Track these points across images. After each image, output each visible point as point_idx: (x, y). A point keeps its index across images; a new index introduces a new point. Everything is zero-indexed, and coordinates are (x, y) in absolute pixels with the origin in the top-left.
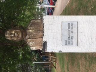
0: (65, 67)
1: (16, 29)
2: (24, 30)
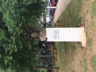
0: (63, 57)
1: (35, 33)
2: (38, 32)
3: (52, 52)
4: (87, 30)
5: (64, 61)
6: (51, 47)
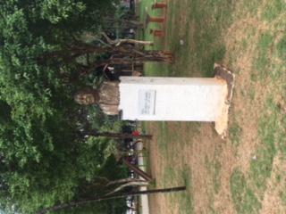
4: (235, 99)
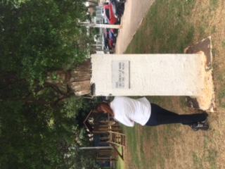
0: (138, 148)
2: (69, 74)
3: (111, 137)
5: (143, 158)
6: (107, 123)
